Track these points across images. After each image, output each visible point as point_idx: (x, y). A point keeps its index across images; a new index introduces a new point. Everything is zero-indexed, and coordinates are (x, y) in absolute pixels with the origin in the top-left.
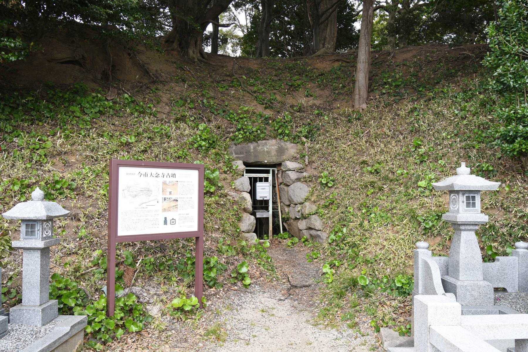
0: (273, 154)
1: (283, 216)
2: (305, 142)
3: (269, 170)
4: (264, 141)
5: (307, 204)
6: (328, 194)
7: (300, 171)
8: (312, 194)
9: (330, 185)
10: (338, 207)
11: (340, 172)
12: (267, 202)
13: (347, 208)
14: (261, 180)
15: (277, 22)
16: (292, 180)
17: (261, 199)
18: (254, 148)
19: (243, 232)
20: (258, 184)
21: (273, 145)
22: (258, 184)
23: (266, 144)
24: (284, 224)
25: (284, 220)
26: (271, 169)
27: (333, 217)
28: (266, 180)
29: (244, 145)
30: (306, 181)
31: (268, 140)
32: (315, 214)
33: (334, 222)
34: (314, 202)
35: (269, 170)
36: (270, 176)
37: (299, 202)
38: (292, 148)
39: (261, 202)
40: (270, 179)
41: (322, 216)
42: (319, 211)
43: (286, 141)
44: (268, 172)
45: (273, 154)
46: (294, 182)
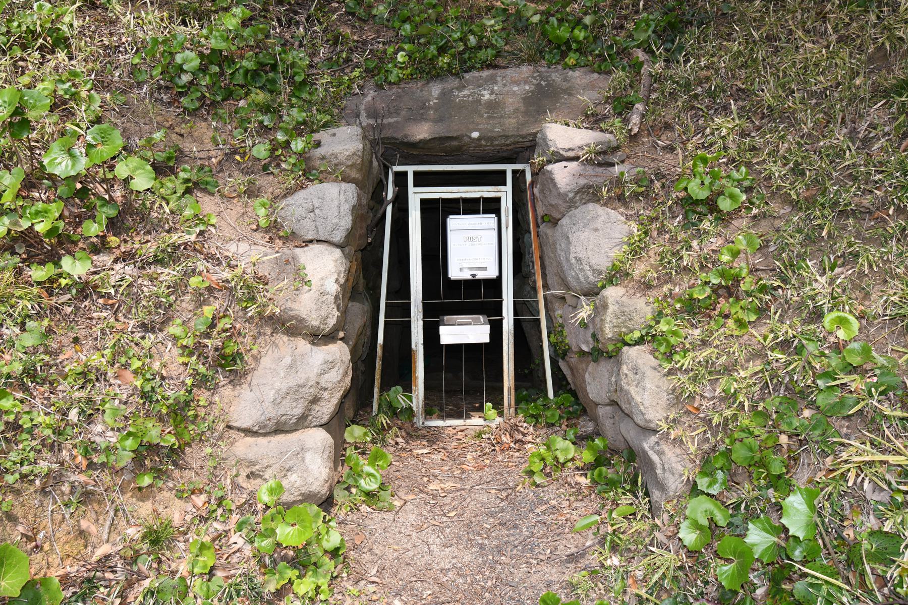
0: (509, 109)
1: (553, 339)
2: (642, 64)
3: (504, 173)
4: (486, 73)
5: (612, 293)
6: (716, 242)
7: (602, 158)
8: (636, 252)
9: (725, 204)
10: (762, 312)
11: (783, 147)
12: (495, 285)
13: (817, 315)
14: (471, 207)
15: (807, 413)
16: (562, 196)
17: (466, 275)
18: (443, 94)
19: (248, 432)
20: (455, 223)
21: (517, 83)
22: (455, 223)
23: (492, 80)
24: (562, 364)
25: (560, 353)
26: (509, 168)
27: (728, 370)
28: (492, 206)
29: (415, 87)
30: (621, 198)
31: (505, 67)
32: (640, 341)
33: (729, 398)
34: (646, 286)
35: (504, 173)
36: (505, 194)
37: (586, 286)
38: (591, 86)
39: (473, 285)
40: (507, 205)
41: (669, 356)
42: (663, 327)
43: (573, 68)
44: (498, 179)
45: (509, 109)
46: (572, 204)
